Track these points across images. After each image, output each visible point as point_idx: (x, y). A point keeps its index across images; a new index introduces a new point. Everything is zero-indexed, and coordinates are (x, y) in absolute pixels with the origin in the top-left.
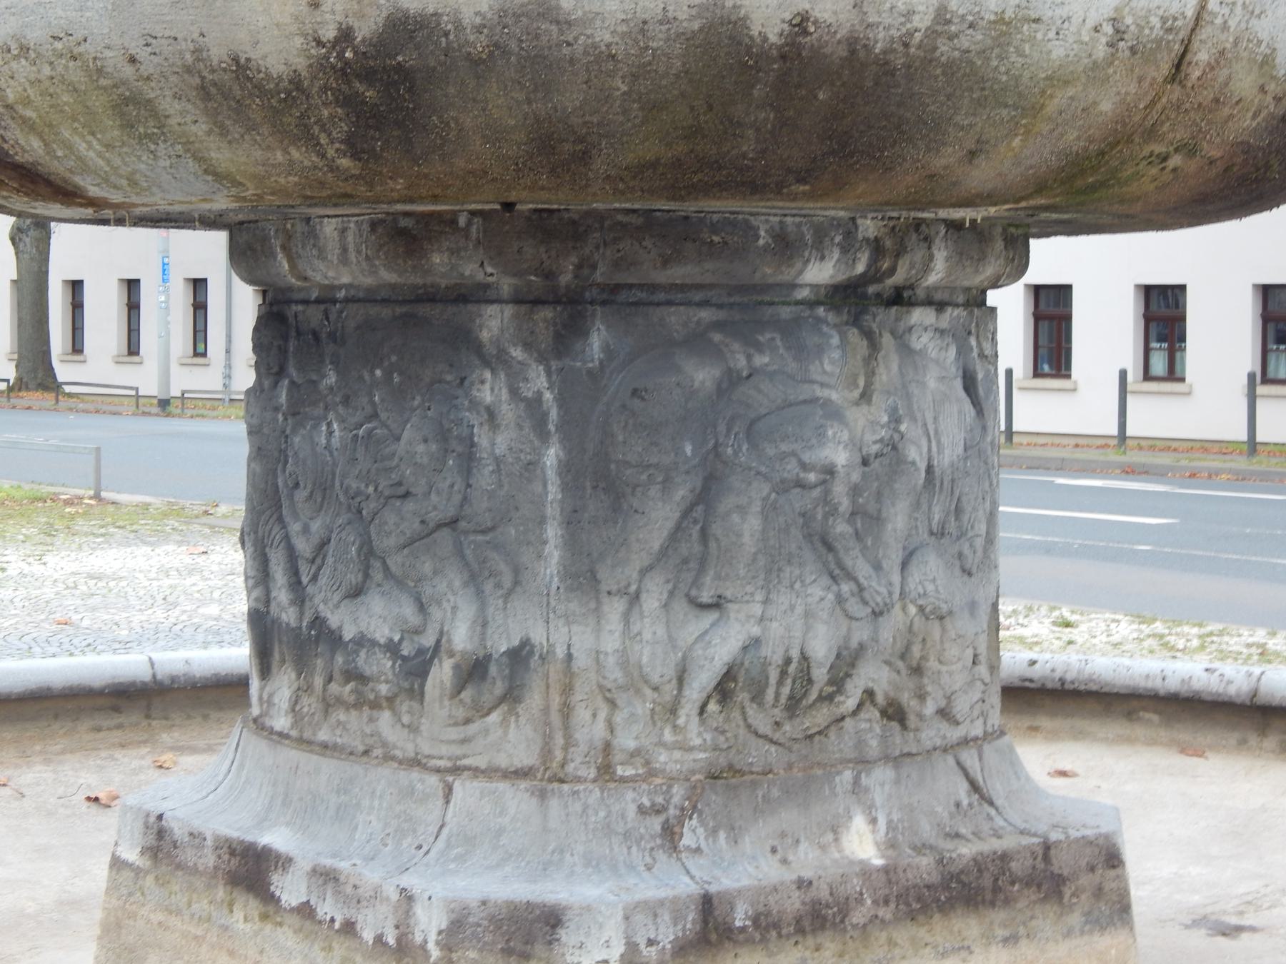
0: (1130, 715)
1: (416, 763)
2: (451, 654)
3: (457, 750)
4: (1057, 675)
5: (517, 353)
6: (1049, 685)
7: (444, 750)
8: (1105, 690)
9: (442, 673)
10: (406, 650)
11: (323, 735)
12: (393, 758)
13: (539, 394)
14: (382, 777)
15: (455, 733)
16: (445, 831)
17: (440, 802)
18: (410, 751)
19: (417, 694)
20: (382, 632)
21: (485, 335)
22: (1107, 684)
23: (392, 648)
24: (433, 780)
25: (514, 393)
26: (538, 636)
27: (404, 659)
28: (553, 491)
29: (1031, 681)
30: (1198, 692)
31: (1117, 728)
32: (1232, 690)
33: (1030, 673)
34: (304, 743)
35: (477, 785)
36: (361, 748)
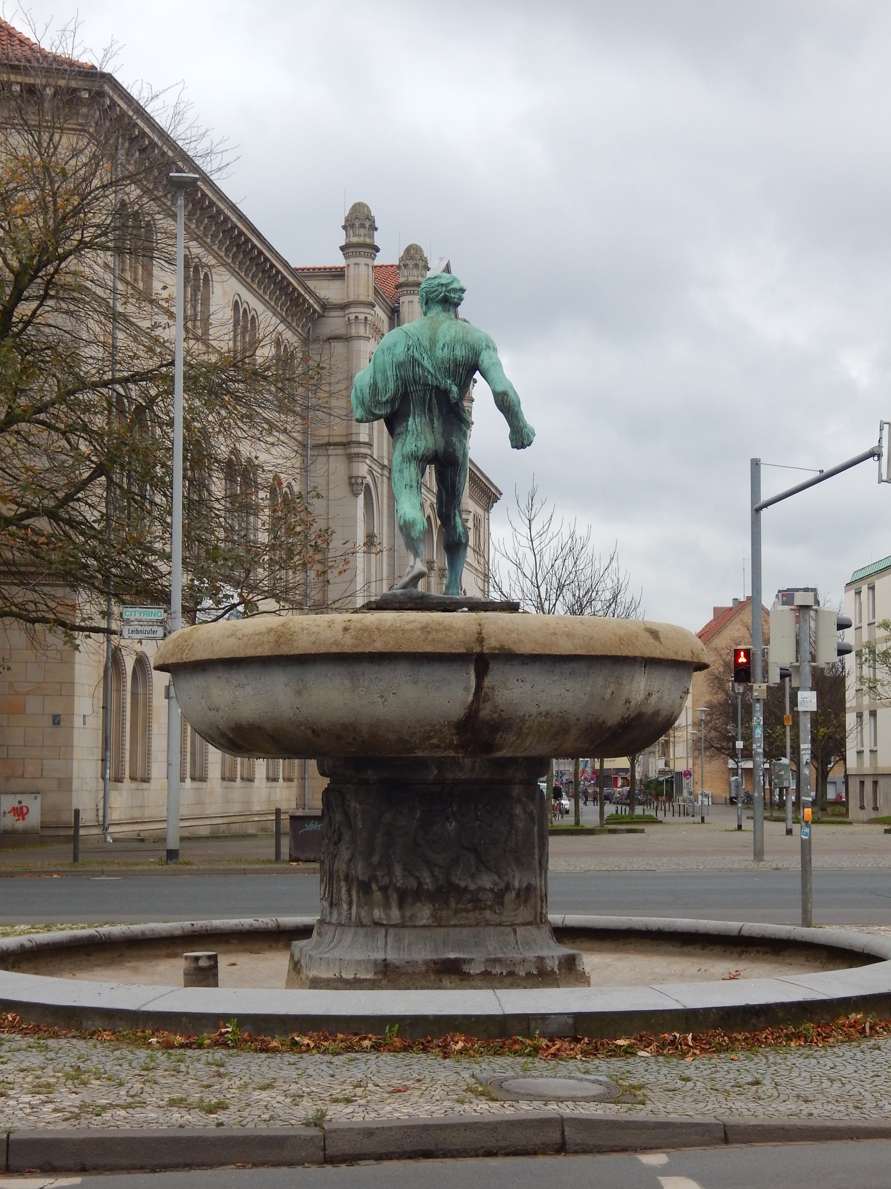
0: (227, 942)
1: (500, 925)
2: (515, 889)
3: (513, 919)
4: (204, 928)
5: (524, 799)
6: (203, 933)
7: (510, 919)
8: (223, 932)
9: (510, 896)
10: (496, 891)
11: (453, 922)
12: (490, 925)
13: (532, 811)
14: (491, 930)
15: (513, 913)
16: (519, 943)
17: (513, 935)
18: (498, 921)
19: (502, 904)
20: (488, 885)
21: (514, 794)
22: (224, 930)
23: (491, 890)
24: (509, 929)
25: (525, 811)
26: (533, 882)
27: (495, 893)
28: (536, 840)
29: (195, 932)
30: (257, 929)
31: (109, 963)
32: (269, 926)
33: (193, 929)
34: (440, 926)
35: (522, 928)
36: (475, 923)
